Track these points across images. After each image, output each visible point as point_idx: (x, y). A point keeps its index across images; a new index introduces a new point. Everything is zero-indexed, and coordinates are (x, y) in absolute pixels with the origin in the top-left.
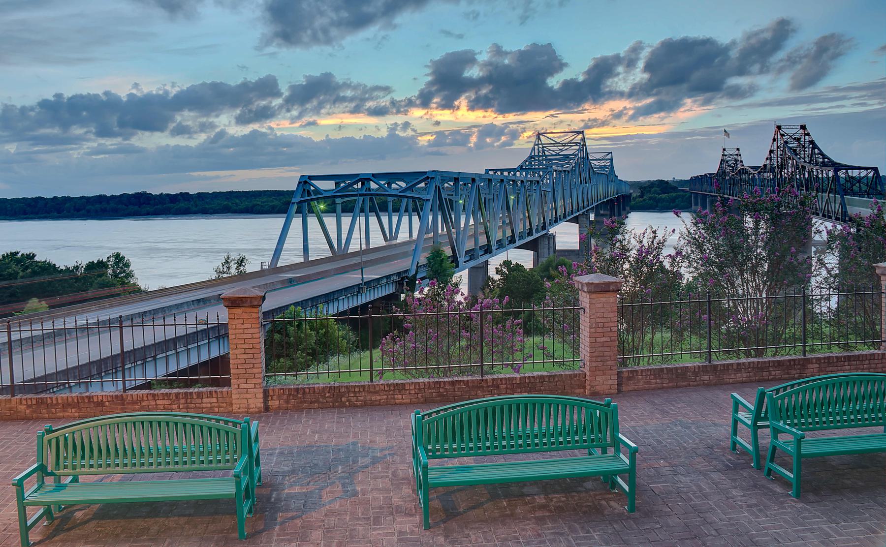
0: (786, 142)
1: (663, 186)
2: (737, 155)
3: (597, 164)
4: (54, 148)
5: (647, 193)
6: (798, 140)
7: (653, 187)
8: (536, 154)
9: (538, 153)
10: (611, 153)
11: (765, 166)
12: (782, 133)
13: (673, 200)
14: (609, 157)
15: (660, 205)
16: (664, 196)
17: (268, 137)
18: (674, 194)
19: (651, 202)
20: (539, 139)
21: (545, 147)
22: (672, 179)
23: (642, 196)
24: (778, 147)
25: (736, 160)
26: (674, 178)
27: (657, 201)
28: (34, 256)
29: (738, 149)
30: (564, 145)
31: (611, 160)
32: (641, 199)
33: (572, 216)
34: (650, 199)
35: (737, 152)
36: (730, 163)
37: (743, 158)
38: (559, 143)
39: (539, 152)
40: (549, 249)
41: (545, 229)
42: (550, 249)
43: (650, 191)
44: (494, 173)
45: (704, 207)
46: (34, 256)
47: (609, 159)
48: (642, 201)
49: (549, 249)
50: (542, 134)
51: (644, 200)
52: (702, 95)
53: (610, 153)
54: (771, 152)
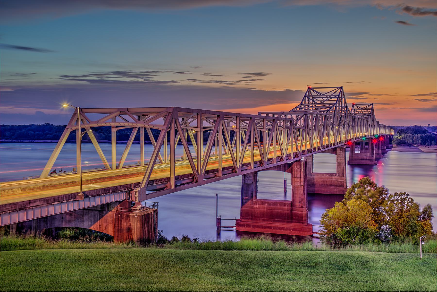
3: (361, 112)
10: (372, 104)
14: (370, 107)
20: (310, 91)
21: (315, 98)
22: (427, 126)
26: (429, 125)
30: (329, 97)
31: (372, 109)
38: (323, 95)
39: (309, 102)
40: (300, 172)
42: (301, 172)
44: (273, 115)
47: (370, 109)
49: (300, 172)
50: (312, 89)
53: (371, 104)
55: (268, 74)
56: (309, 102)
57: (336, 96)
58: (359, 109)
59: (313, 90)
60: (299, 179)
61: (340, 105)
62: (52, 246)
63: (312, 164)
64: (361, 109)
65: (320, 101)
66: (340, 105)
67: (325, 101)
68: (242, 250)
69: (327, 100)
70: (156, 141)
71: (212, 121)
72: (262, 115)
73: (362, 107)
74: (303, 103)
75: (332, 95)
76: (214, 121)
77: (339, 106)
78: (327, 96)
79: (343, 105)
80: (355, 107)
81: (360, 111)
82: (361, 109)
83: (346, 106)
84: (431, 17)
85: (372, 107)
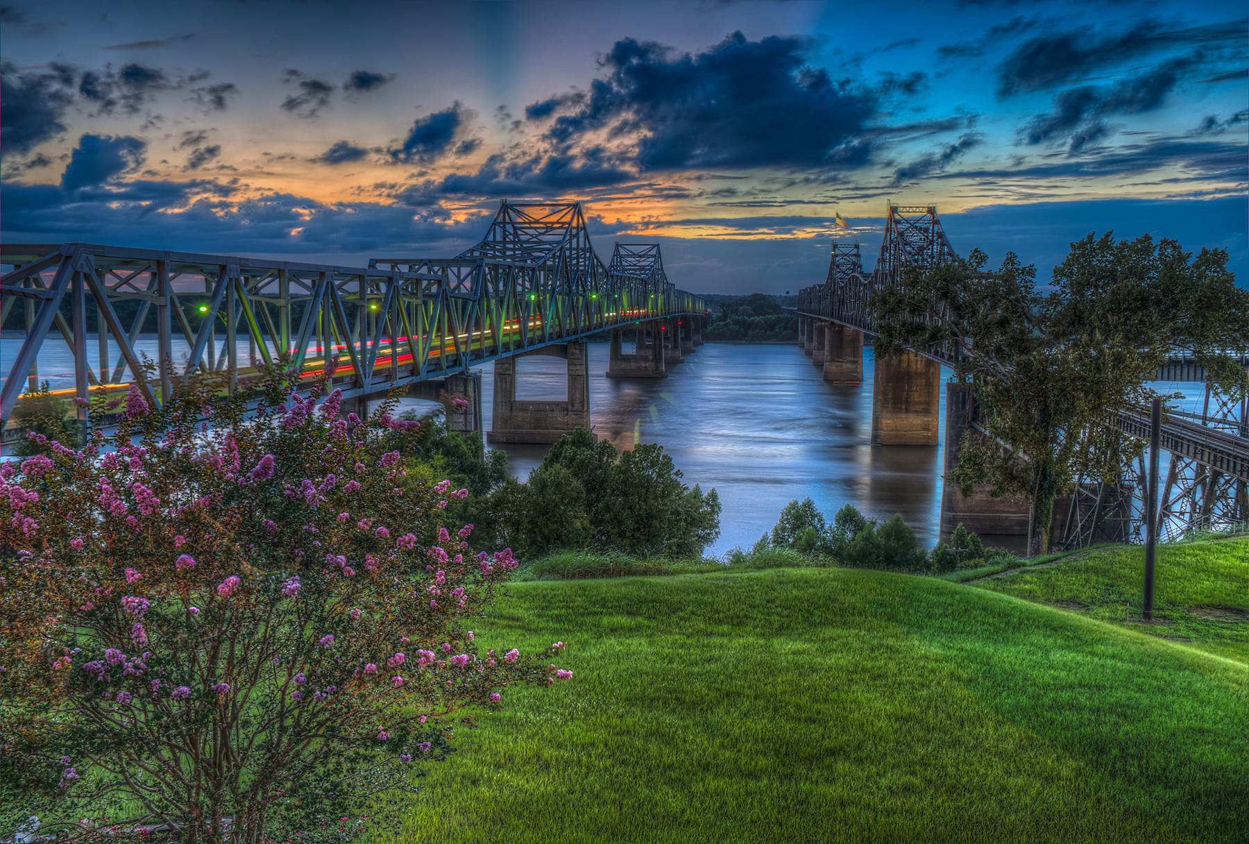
0: (901, 234)
1: (760, 303)
2: (854, 255)
4: (1186, 198)
5: (732, 313)
6: (926, 230)
7: (741, 305)
8: (499, 238)
9: (504, 239)
10: (658, 245)
11: (876, 272)
12: (897, 217)
13: (772, 326)
14: (654, 252)
15: (750, 332)
16: (757, 319)
17: (301, 219)
18: (773, 317)
19: (736, 328)
21: (520, 229)
23: (722, 319)
24: (891, 242)
25: (854, 263)
26: (788, 293)
27: (747, 326)
28: (796, 503)
29: (857, 247)
32: (722, 323)
33: (543, 345)
34: (736, 322)
35: (855, 251)
36: (843, 268)
37: (863, 261)
41: (460, 365)
43: (736, 311)
44: (393, 267)
45: (810, 339)
46: (796, 503)
48: (722, 327)
51: (726, 325)
52: (1066, 133)
53: (654, 246)
54: (884, 249)
55: (313, 161)
56: (504, 239)
57: (564, 223)
58: (629, 256)
59: (515, 211)
60: (463, 416)
61: (574, 245)
62: (635, 562)
63: (875, 404)
64: (634, 255)
65: (527, 234)
66: (574, 245)
67: (541, 234)
68: (780, 565)
69: (543, 234)
70: (56, 317)
71: (308, 282)
72: (380, 267)
73: (636, 249)
74: (491, 238)
75: (558, 222)
76: (314, 282)
77: (570, 249)
78: (545, 223)
79: (582, 245)
80: (622, 252)
81: (632, 259)
82: (634, 255)
83: (591, 248)
84: (1241, 83)
85: (659, 251)
